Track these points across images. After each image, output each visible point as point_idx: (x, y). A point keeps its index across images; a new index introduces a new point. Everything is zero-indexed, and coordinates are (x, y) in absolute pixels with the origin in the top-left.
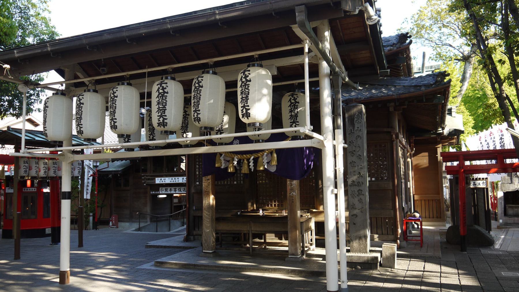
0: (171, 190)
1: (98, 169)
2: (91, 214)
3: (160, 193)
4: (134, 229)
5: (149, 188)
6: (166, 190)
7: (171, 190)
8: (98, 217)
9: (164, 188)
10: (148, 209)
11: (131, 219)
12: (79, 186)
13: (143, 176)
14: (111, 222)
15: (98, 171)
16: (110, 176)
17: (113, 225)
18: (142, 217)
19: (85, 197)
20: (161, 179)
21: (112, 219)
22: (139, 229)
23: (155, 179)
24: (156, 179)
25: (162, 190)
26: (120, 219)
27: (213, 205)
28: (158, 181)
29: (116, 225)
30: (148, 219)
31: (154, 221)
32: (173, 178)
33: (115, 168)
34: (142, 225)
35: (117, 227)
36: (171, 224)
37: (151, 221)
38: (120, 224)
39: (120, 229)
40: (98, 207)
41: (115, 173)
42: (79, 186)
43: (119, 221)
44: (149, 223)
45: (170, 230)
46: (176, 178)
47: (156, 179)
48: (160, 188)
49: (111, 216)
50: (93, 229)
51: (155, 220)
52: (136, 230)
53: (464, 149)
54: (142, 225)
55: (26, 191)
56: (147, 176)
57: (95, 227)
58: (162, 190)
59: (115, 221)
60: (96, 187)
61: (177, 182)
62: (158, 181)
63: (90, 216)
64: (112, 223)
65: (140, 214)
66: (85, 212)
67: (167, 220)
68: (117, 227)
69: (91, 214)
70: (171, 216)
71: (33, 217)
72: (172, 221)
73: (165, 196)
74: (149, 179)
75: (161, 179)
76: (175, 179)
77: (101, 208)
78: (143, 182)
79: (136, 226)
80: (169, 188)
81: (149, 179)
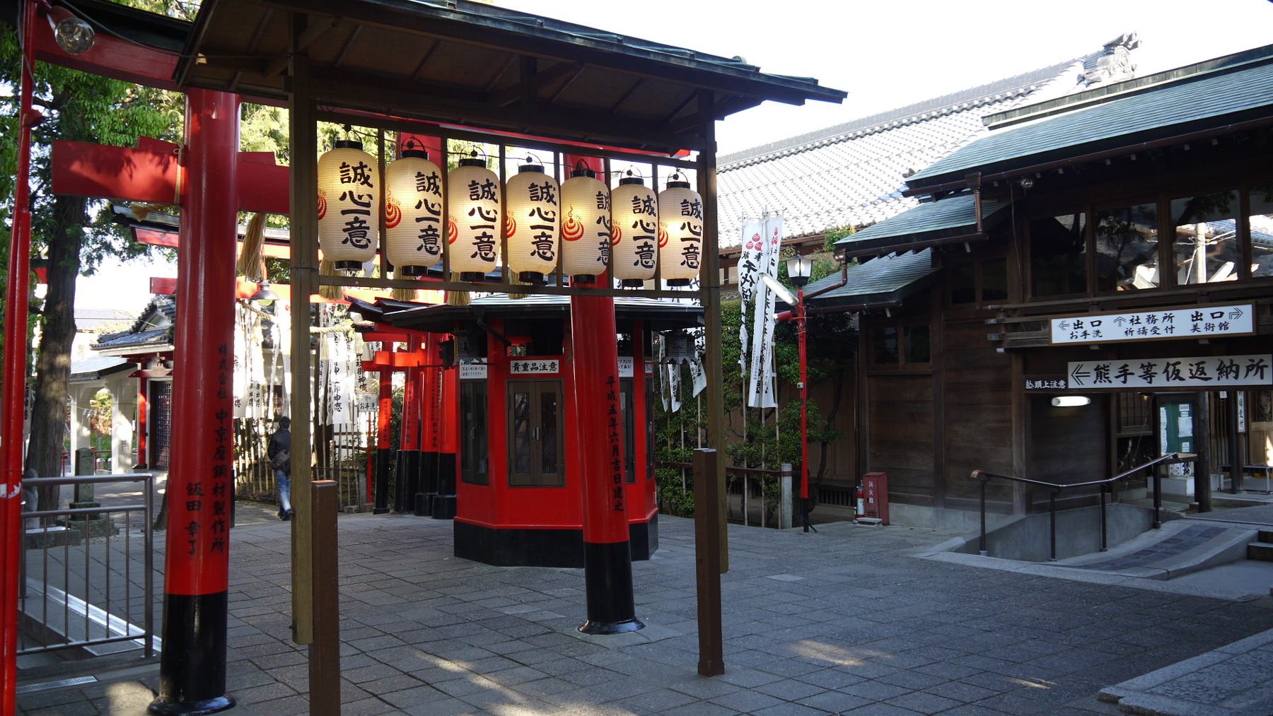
0: (1125, 373)
1: (809, 290)
2: (787, 468)
3: (1073, 384)
4: (960, 541)
5: (1016, 366)
6: (1101, 373)
7: (1125, 373)
8: (814, 475)
9: (1089, 366)
10: (1013, 456)
11: (940, 491)
12: (742, 362)
13: (993, 314)
14: (860, 502)
15: (807, 300)
16: (855, 322)
17: (869, 513)
18: (987, 490)
19: (752, 403)
20: (1078, 325)
21: (866, 488)
22: (982, 544)
23: (1047, 324)
24: (1055, 323)
25: (1079, 375)
26: (897, 491)
27: (108, 386)
28: (1062, 331)
29: (880, 512)
30: (1017, 499)
31: (1041, 509)
32: (1143, 316)
33: (871, 285)
34: (994, 522)
35: (886, 523)
36: (1109, 521)
37: (1029, 508)
38: (895, 509)
39: (896, 529)
40: (810, 440)
41: (871, 308)
42: (742, 362)
43: (894, 499)
44: (1019, 515)
45: (1103, 547)
46: (1159, 315)
47: (1055, 323)
48: (1072, 366)
49: (859, 476)
50: (795, 524)
51: (1046, 501)
52: (968, 548)
53: (240, 507)
54: (994, 522)
55: (521, 371)
56: (1008, 313)
57: (803, 519)
58: (1085, 377)
59: (878, 497)
60: (798, 366)
61: (1163, 334)
62: (1062, 331)
63: (781, 474)
64: (866, 503)
65: (987, 477)
66: (766, 461)
67: (1092, 502)
68: (886, 523)
69: (787, 468)
70: (1106, 488)
71: (550, 479)
72: (1111, 507)
73: (1082, 401)
74: (1015, 327)
75: (1078, 325)
76: (1152, 320)
77: (824, 445)
78: (993, 337)
79: (964, 524)
80: (1114, 367)
81: (1015, 327)
